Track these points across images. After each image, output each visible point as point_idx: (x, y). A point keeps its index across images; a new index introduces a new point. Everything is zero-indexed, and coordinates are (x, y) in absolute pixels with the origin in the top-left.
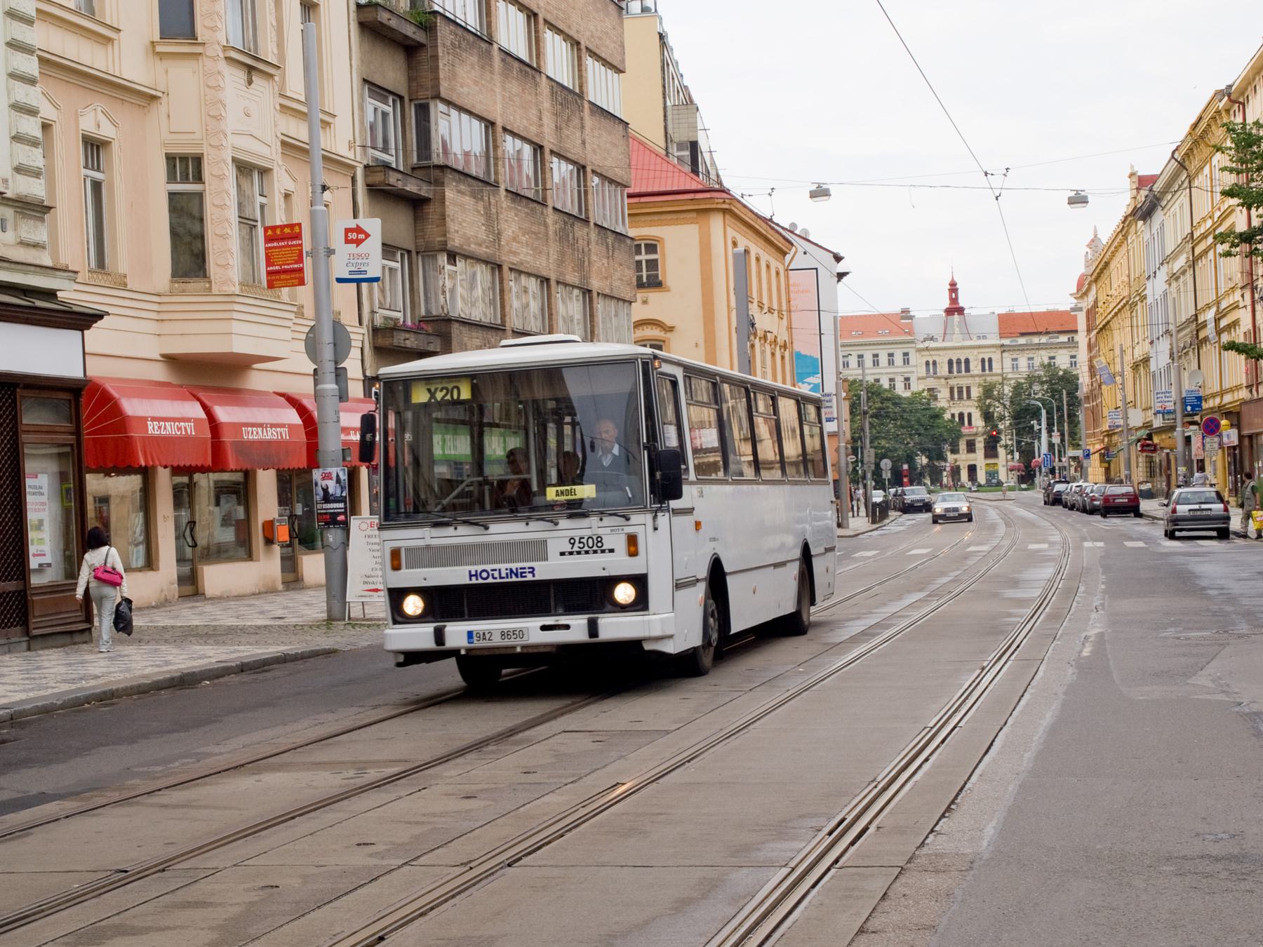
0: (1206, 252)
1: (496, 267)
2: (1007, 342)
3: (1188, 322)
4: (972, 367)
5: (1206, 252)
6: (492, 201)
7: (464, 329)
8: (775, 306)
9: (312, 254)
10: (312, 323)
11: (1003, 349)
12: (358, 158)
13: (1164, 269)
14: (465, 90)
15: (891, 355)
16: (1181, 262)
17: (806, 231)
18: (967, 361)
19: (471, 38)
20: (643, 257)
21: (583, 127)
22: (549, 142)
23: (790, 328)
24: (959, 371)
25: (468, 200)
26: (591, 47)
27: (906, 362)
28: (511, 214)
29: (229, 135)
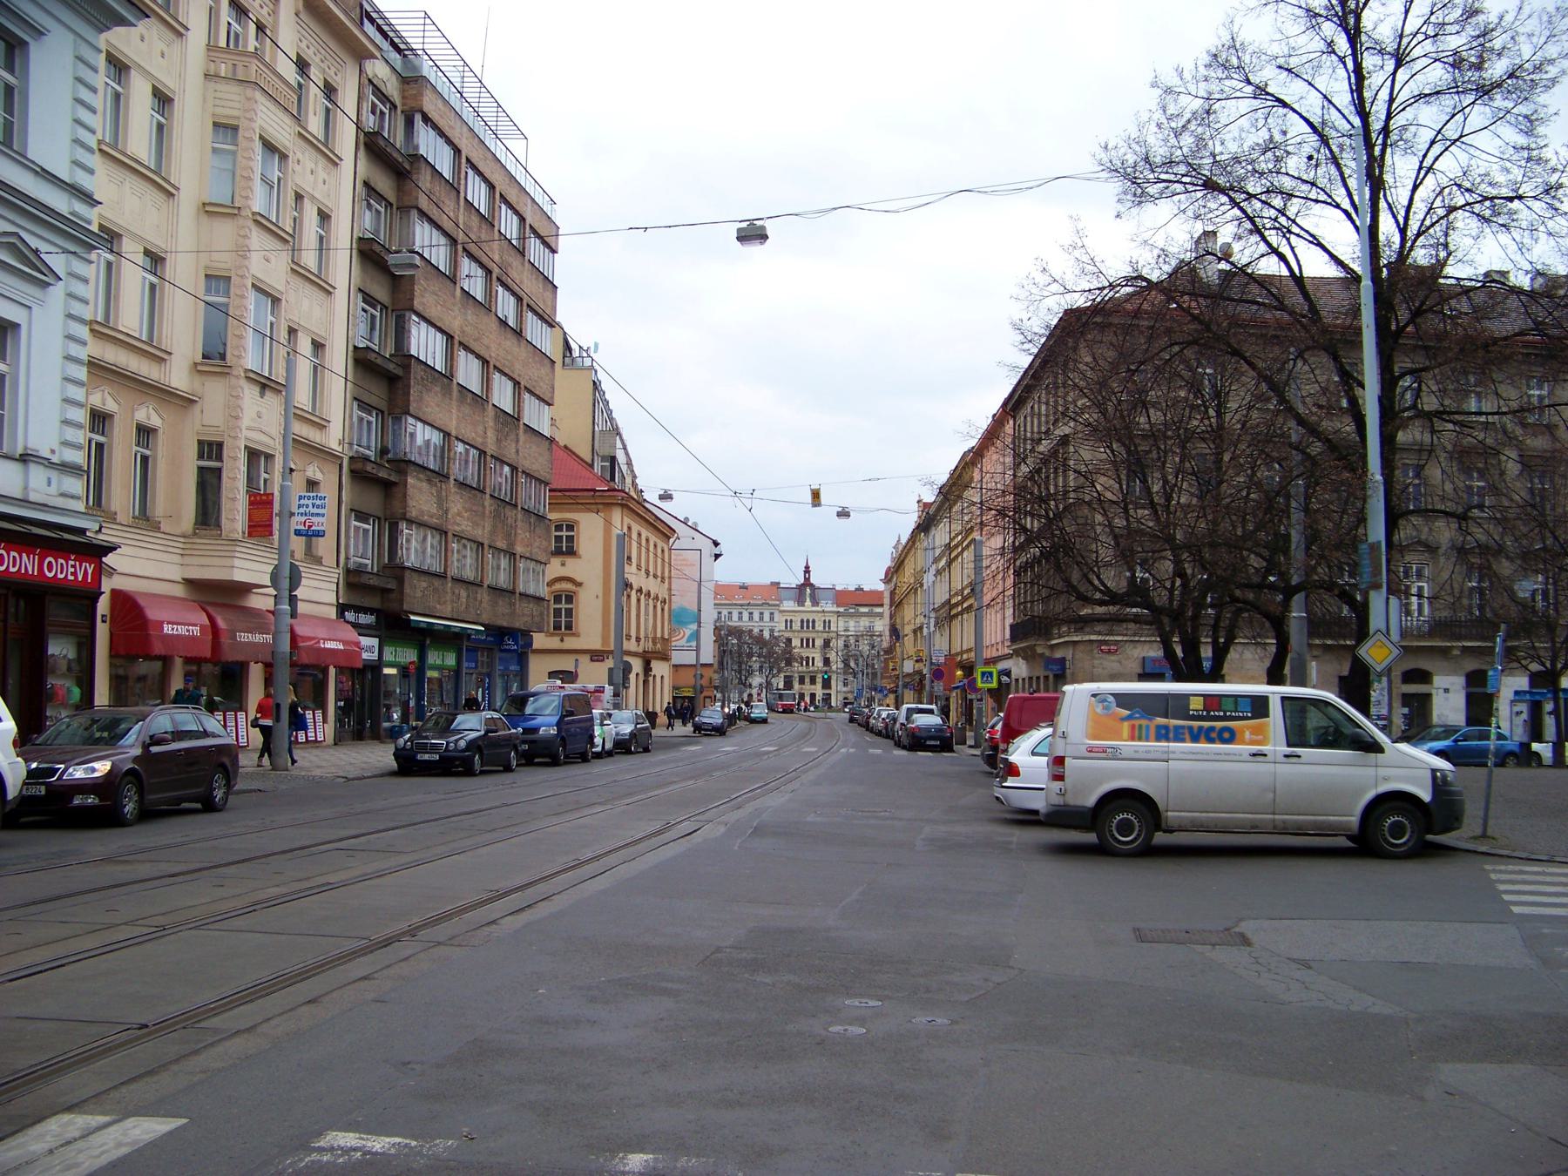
0: (957, 557)
1: (443, 532)
2: (841, 610)
3: (943, 605)
4: (817, 625)
5: (957, 557)
6: (444, 487)
7: (415, 575)
8: (659, 574)
9: (279, 515)
10: (276, 563)
12: (345, 453)
13: (934, 566)
14: (429, 410)
16: (943, 563)
17: (695, 524)
18: (814, 621)
19: (437, 375)
20: (564, 533)
21: (517, 441)
22: (491, 448)
24: (808, 627)
25: (425, 485)
26: (528, 386)
27: (772, 619)
28: (458, 497)
29: (244, 430)
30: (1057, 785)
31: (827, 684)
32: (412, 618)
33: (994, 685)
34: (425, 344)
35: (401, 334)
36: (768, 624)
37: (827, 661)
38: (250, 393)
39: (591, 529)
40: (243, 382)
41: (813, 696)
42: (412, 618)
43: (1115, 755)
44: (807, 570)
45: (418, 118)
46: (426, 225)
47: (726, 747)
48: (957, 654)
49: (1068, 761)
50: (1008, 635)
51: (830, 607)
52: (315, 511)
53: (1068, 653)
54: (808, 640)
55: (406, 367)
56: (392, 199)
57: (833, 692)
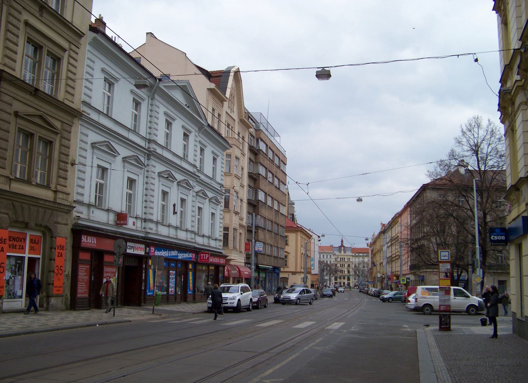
0: (394, 243)
2: (354, 254)
3: (389, 257)
11: (353, 256)
13: (386, 245)
15: (327, 256)
16: (389, 244)
18: (344, 258)
23: (310, 253)
24: (342, 260)
25: (262, 232)
27: (330, 257)
30: (416, 303)
31: (349, 279)
32: (260, 265)
33: (405, 283)
34: (261, 196)
35: (256, 194)
36: (331, 260)
37: (349, 272)
38: (234, 215)
39: (292, 237)
40: (233, 214)
41: (344, 283)
42: (260, 265)
43: (425, 298)
44: (342, 241)
45: (260, 140)
46: (262, 166)
47: (335, 298)
48: (394, 272)
49: (418, 299)
50: (409, 268)
51: (349, 253)
52: (260, 246)
53: (424, 274)
54: (342, 265)
55: (258, 203)
56: (254, 161)
57: (351, 282)
